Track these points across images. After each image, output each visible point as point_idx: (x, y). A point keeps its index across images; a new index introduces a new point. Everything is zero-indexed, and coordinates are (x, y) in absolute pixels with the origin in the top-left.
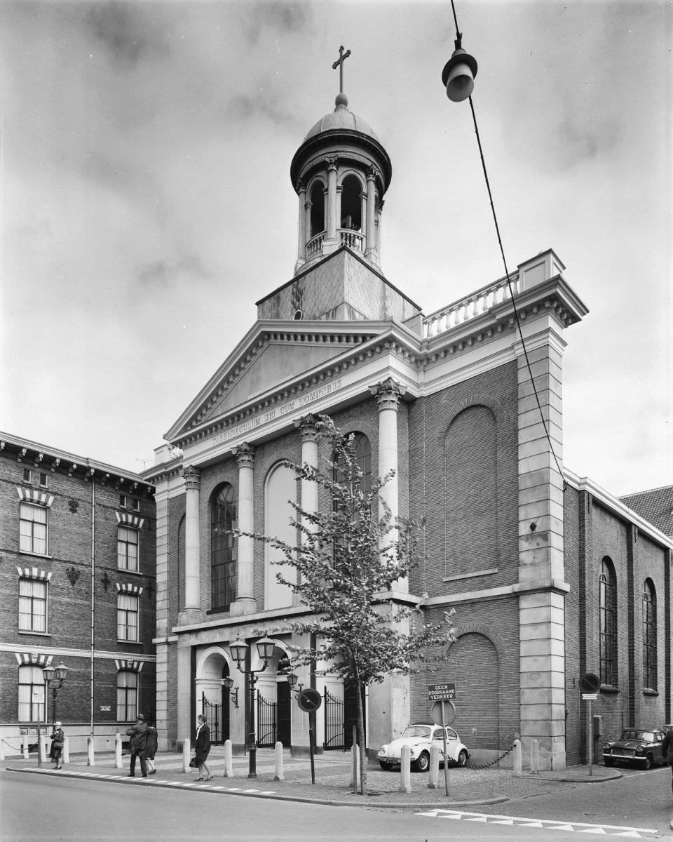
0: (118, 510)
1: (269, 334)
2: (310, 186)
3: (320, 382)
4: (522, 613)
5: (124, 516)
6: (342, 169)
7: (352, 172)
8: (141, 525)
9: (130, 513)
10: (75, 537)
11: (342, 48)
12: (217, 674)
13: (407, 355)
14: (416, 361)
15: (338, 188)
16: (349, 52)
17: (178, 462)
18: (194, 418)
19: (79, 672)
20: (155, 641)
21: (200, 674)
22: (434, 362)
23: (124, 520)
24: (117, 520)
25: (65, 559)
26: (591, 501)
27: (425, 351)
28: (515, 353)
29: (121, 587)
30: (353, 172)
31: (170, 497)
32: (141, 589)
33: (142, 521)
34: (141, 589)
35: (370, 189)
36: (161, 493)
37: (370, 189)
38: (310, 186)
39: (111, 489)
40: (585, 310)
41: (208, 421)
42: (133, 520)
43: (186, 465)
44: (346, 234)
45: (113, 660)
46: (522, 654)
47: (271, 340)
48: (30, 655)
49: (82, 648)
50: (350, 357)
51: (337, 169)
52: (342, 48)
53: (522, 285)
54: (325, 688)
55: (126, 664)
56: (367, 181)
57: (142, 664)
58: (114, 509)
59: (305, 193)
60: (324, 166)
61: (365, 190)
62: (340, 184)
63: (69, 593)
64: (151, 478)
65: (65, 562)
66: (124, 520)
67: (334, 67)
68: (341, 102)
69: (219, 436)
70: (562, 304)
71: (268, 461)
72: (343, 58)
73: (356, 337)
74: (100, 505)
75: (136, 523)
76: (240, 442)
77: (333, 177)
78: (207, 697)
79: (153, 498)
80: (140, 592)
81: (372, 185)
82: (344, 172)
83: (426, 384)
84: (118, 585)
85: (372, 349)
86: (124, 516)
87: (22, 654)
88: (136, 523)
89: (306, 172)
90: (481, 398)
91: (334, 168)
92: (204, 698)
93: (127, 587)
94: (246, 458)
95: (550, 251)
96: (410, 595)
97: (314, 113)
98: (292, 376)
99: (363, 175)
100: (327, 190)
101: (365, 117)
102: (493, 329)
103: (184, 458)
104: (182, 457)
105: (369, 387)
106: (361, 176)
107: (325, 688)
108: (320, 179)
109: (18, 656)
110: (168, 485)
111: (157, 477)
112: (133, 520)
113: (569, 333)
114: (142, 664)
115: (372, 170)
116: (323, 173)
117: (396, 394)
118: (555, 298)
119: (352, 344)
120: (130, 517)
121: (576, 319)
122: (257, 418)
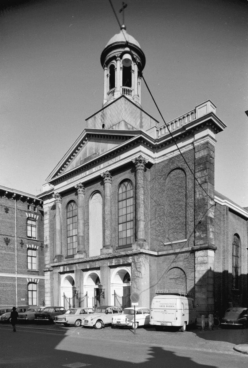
0: (27, 212)
2: (109, 66)
5: (29, 214)
9: (32, 213)
10: (8, 224)
14: (153, 148)
15: (121, 68)
19: (11, 284)
24: (26, 216)
25: (3, 234)
26: (228, 210)
29: (29, 246)
33: (38, 216)
34: (38, 247)
35: (135, 68)
37: (135, 68)
42: (34, 216)
45: (26, 278)
48: (31, 279)
49: (11, 273)
55: (32, 280)
57: (39, 280)
58: (25, 211)
63: (5, 249)
65: (3, 235)
74: (18, 209)
81: (136, 66)
84: (27, 245)
87: (29, 279)
88: (35, 217)
93: (31, 246)
103: (55, 189)
104: (54, 189)
107: (115, 291)
109: (27, 279)
114: (39, 280)
117: (144, 163)
120: (32, 215)
121: (221, 130)
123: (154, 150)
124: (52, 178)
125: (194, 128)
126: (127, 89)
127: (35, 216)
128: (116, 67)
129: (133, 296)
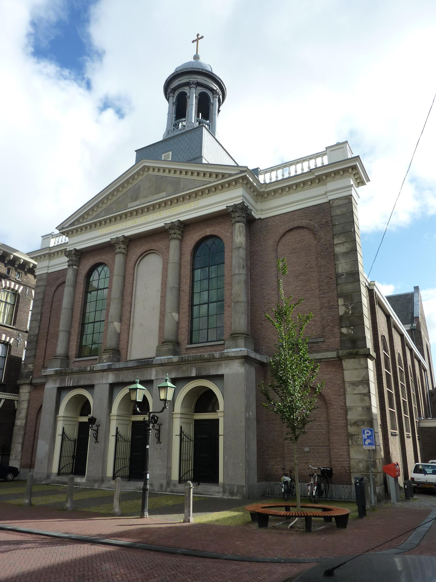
1: (149, 168)
2: (177, 93)
3: (167, 206)
4: (346, 373)
6: (199, 88)
7: (204, 90)
8: (20, 291)
11: (198, 35)
12: (35, 58)
13: (252, 190)
16: (202, 37)
17: (65, 246)
18: (82, 217)
20: (19, 382)
21: (62, 412)
22: (266, 198)
23: (8, 286)
27: (263, 190)
28: (327, 197)
30: (204, 91)
31: (49, 271)
32: (12, 339)
34: (12, 339)
36: (40, 268)
38: (177, 93)
39: (348, 174)
40: (368, 180)
42: (15, 286)
43: (70, 248)
47: (149, 172)
50: (232, 180)
52: (198, 35)
53: (329, 159)
59: (173, 97)
64: (34, 257)
66: (8, 286)
67: (202, 37)
68: (196, 57)
69: (111, 227)
70: (358, 173)
71: (138, 250)
72: (197, 40)
73: (217, 175)
75: (16, 288)
76: (119, 235)
78: (67, 432)
79: (34, 271)
80: (11, 342)
82: (201, 90)
83: (262, 210)
85: (229, 183)
86: (8, 282)
90: (304, 222)
91: (195, 86)
92: (63, 432)
94: (123, 246)
95: (347, 142)
96: (219, 373)
97: (182, 58)
99: (212, 94)
100: (189, 97)
101: (210, 61)
102: (312, 181)
106: (210, 94)
108: (185, 91)
110: (49, 262)
111: (40, 256)
112: (15, 286)
113: (361, 190)
118: (354, 168)
119: (212, 179)
123: (257, 199)
125: (327, 175)
127: (17, 286)
128: (188, 95)
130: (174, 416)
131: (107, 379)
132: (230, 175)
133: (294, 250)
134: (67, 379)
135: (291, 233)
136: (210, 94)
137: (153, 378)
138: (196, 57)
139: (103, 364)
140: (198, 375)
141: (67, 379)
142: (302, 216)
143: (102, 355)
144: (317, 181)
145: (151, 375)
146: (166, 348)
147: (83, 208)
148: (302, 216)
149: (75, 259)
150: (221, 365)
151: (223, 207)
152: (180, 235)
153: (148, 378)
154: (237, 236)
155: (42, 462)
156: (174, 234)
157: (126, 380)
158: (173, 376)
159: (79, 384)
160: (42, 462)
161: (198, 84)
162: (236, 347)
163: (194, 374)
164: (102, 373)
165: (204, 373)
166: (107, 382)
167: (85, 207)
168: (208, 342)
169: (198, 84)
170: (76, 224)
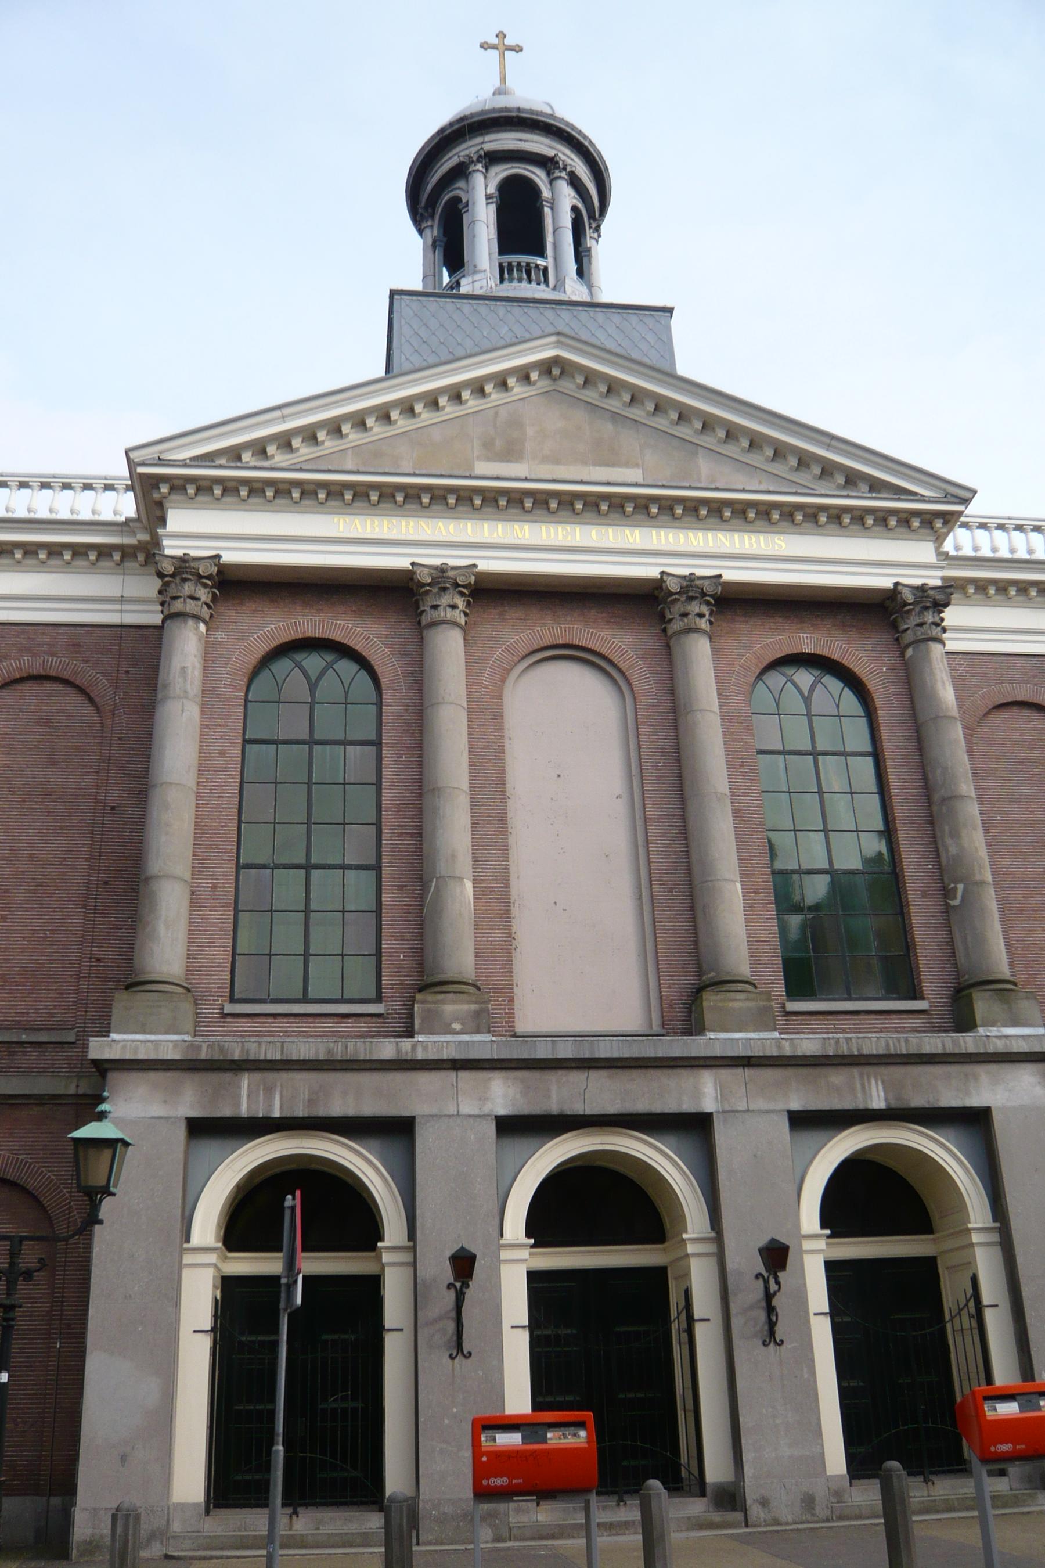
15: (488, 197)
35: (561, 203)
41: (301, 470)
44: (519, 264)
46: (696, 1317)
51: (487, 170)
52: (484, 46)
54: (513, 1327)
56: (551, 182)
59: (432, 226)
60: (461, 172)
61: (546, 193)
62: (492, 189)
77: (478, 180)
82: (500, 172)
89: (433, 193)
90: (54, 665)
95: (127, 453)
96: (975, 1101)
98: (763, 487)
105: (413, 564)
106: (538, 176)
107: (513, 1327)
115: (558, 163)
116: (461, 184)
122: (587, 1498)
124: (192, 459)
126: (515, 264)
129: (273, 1338)
130: (505, 1255)
131: (484, 1099)
132: (923, 499)
133: (1021, 763)
134: (244, 1092)
135: (1026, 713)
136: (538, 176)
137: (708, 1105)
138: (499, 92)
139: (449, 1038)
140: (894, 1104)
141: (244, 1092)
142: (1034, 677)
143: (443, 1002)
144: (141, 558)
145: (697, 1094)
146: (750, 1004)
147: (277, 414)
148: (1034, 677)
149: (204, 598)
150: (976, 1078)
151: (884, 581)
152: (209, 607)
153: (687, 1106)
154: (943, 682)
155: (123, 1459)
156: (193, 598)
157: (579, 1108)
158: (795, 1105)
159: (322, 1112)
160: (123, 1459)
161: (493, 158)
162: (1015, 1023)
163: (878, 1101)
164: (453, 1074)
165: (918, 1101)
166: (487, 1108)
167: (286, 411)
168: (305, 1000)
169: (493, 158)
170: (223, 461)
